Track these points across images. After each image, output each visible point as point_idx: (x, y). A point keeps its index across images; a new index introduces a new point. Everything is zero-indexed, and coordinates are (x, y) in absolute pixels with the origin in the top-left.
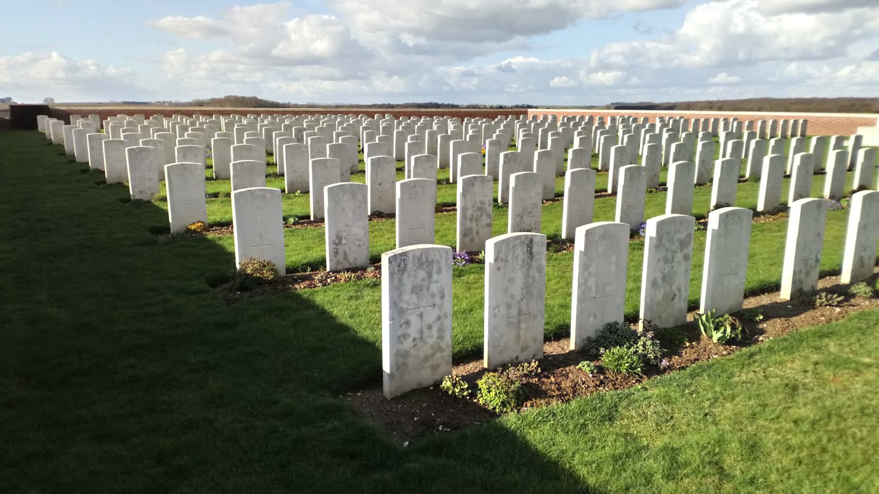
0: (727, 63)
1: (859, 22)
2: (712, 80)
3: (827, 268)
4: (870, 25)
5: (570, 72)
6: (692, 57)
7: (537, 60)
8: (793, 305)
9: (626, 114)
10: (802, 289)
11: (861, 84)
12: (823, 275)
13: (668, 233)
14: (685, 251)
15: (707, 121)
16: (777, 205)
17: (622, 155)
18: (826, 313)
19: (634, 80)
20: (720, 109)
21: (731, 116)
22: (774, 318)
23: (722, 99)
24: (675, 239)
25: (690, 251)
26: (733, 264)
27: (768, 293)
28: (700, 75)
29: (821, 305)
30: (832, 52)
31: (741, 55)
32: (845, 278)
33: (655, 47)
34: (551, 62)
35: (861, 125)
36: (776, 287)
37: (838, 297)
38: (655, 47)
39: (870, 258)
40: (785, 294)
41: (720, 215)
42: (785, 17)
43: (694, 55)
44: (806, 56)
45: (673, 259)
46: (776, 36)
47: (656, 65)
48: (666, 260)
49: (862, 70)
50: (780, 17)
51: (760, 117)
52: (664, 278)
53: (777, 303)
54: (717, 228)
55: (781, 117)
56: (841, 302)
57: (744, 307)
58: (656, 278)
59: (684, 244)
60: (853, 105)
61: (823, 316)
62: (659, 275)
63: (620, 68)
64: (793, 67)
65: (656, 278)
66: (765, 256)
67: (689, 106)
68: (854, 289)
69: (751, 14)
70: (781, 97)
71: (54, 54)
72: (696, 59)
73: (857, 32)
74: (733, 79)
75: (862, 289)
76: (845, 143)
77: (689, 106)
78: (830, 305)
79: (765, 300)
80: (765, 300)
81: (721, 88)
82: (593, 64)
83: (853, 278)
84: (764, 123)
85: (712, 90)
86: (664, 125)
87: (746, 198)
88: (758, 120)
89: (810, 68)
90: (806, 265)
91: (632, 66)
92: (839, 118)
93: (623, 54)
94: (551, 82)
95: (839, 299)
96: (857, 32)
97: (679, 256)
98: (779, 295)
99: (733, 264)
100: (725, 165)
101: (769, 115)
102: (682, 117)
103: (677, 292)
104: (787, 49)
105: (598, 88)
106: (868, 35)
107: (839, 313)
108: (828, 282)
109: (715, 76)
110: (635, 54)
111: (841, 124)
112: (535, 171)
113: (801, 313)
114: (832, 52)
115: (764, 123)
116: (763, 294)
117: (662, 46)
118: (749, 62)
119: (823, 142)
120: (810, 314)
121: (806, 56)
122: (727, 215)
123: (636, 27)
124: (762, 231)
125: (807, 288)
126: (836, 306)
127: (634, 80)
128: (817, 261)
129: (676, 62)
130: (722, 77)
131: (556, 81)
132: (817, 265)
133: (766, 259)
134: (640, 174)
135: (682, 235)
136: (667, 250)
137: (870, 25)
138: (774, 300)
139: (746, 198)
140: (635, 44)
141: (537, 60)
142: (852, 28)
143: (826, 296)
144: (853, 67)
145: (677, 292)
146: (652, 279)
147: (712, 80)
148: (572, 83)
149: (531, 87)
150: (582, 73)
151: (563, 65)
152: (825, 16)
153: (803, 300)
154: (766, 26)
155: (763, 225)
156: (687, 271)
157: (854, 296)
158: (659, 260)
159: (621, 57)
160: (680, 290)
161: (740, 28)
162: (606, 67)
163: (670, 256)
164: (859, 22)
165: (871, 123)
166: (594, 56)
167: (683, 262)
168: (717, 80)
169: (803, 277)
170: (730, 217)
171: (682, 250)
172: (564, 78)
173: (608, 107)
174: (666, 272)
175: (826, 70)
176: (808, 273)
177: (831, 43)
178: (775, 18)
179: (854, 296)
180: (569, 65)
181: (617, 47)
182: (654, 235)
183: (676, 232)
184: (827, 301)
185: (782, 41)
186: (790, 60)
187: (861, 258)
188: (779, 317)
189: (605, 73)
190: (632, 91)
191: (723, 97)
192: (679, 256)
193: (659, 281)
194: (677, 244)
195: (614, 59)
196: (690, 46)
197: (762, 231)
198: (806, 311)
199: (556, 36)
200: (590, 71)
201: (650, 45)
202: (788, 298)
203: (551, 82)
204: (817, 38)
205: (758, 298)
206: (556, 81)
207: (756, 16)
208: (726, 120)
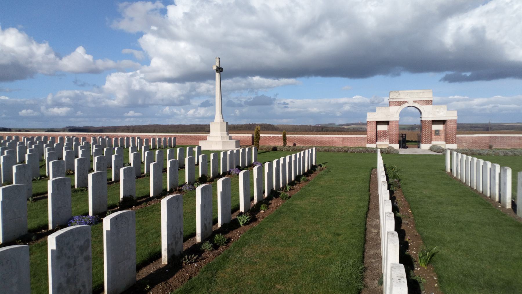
0: (133, 105)
1: (193, 89)
2: (126, 115)
4: (198, 90)
5: (34, 107)
6: (113, 101)
7: (7, 98)
10: (174, 254)
11: (198, 118)
12: (185, 240)
14: (85, 254)
15: (122, 139)
16: (161, 191)
18: (191, 267)
19: (79, 113)
20: (133, 131)
21: (137, 136)
22: (157, 284)
23: (134, 125)
25: (90, 252)
27: (155, 260)
28: (119, 112)
29: (186, 264)
30: (184, 102)
33: (90, 94)
34: (19, 100)
35: (201, 140)
37: (195, 256)
38: (90, 94)
39: (209, 223)
41: (111, 220)
42: (159, 84)
43: (114, 100)
44: (172, 104)
45: (75, 262)
47: (93, 105)
48: (68, 266)
49: (198, 111)
51: (152, 136)
52: (68, 281)
54: (109, 229)
55: (163, 136)
56: (197, 258)
57: (138, 279)
58: (60, 284)
60: (197, 128)
61: (187, 272)
63: (68, 105)
64: (167, 109)
65: (60, 284)
67: (115, 129)
69: (142, 80)
70: (162, 124)
71: (80, 50)
72: (115, 102)
73: (193, 93)
74: (136, 114)
75: (207, 246)
76: (194, 149)
77: (115, 129)
78: (191, 263)
79: (152, 268)
80: (152, 268)
81: (132, 119)
82: (50, 103)
85: (127, 120)
87: (144, 188)
88: (150, 138)
91: (76, 104)
92: (190, 136)
94: (20, 113)
96: (193, 93)
97: (80, 259)
98: (161, 262)
99: (126, 252)
100: (126, 172)
103: (81, 288)
104: (163, 100)
105: (55, 117)
106: (198, 95)
107: (196, 267)
109: (128, 112)
110: (77, 98)
111: (191, 139)
112: (26, 163)
113: (174, 275)
114: (184, 102)
117: (93, 94)
118: (144, 106)
119: (183, 151)
120: (180, 272)
122: (116, 218)
123: (75, 82)
124: (152, 212)
125: (177, 253)
126: (194, 262)
127: (79, 113)
129: (104, 104)
130: (131, 113)
134: (65, 184)
135: (81, 242)
136: (69, 258)
137: (198, 90)
138: (158, 267)
140: (78, 92)
141: (7, 98)
142: (191, 91)
143: (188, 258)
144: (194, 110)
145: (81, 288)
147: (126, 115)
148: (36, 114)
149: (4, 116)
150: (43, 108)
151: (27, 102)
152: (177, 84)
153: (176, 261)
154: (152, 87)
155: (153, 206)
156: (88, 269)
157: (203, 251)
158: (62, 267)
159: (68, 99)
160: (84, 286)
162: (60, 105)
164: (193, 89)
165: (205, 139)
166: (50, 98)
168: (129, 115)
172: (29, 111)
173: (64, 130)
174: (69, 275)
176: (176, 243)
177: (182, 98)
178: (154, 84)
179: (203, 251)
180: (32, 102)
181: (65, 93)
183: (75, 241)
184: (189, 260)
185: (159, 96)
187: (205, 224)
188: (160, 282)
190: (79, 120)
191: (134, 124)
192: (80, 259)
194: (77, 250)
195: (64, 100)
196: (111, 96)
197: (152, 212)
199: (17, 84)
200: (48, 107)
201: (86, 93)
202: (167, 263)
203: (20, 113)
204: (175, 95)
205: (148, 267)
207: (144, 82)
208: (133, 139)
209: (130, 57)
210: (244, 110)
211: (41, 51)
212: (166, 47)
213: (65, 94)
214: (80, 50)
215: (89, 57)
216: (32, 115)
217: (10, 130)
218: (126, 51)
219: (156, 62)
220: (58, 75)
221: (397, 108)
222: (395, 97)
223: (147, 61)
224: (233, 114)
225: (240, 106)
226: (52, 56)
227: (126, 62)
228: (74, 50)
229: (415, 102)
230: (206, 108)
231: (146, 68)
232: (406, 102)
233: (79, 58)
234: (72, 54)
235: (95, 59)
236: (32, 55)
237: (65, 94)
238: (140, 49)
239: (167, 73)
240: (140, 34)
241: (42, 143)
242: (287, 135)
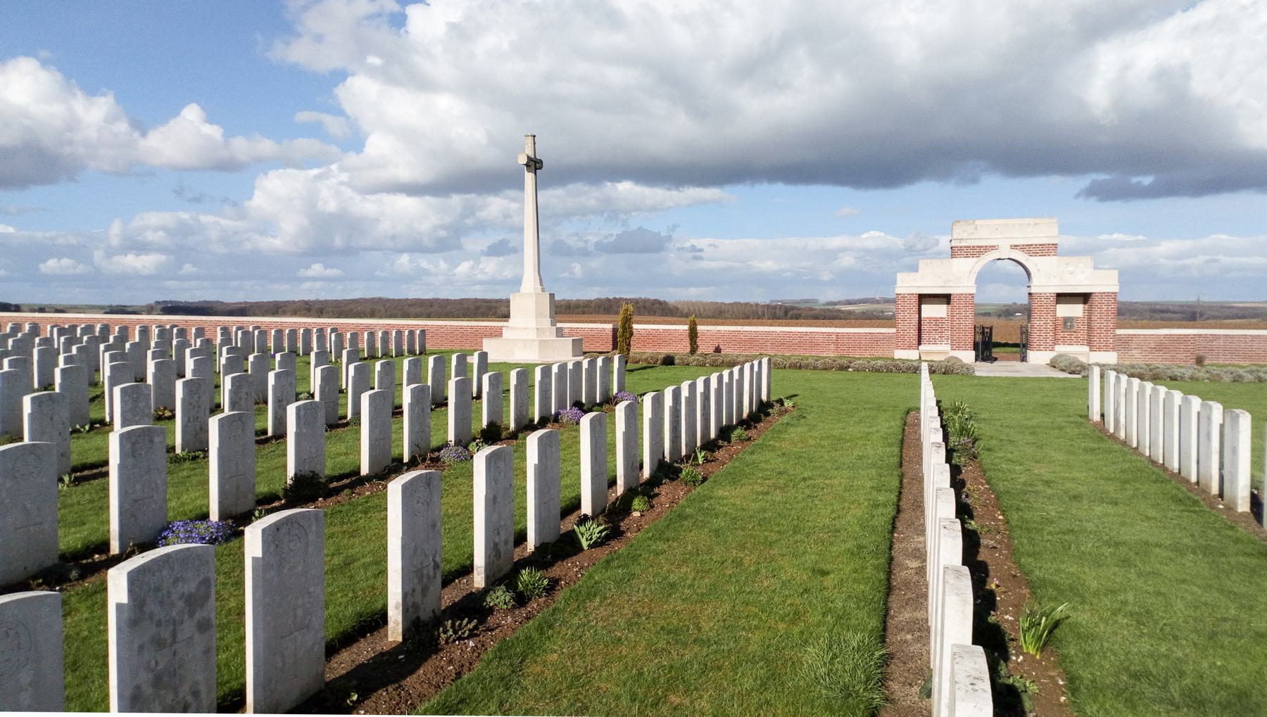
0: (320, 251)
1: (470, 211)
3: (453, 566)
4: (482, 215)
5: (78, 252)
6: (272, 240)
7: (11, 230)
8: (407, 653)
9: (169, 321)
10: (418, 618)
12: (447, 581)
13: (157, 589)
14: (199, 615)
15: (293, 333)
16: (389, 462)
17: (136, 401)
18: (458, 649)
19: (188, 268)
21: (329, 325)
22: (376, 691)
23: (322, 299)
24: (174, 597)
26: (299, 612)
27: (371, 632)
29: (447, 642)
30: (446, 243)
31: (338, 242)
32: (479, 580)
33: (215, 223)
35: (486, 336)
36: (380, 619)
37: (469, 622)
38: (215, 223)
39: (506, 542)
40: (395, 630)
41: (264, 531)
43: (274, 237)
44: (416, 247)
46: (377, 220)
47: (222, 250)
48: (158, 643)
50: (379, 196)
51: (368, 326)
52: (157, 682)
53: (382, 654)
55: (393, 326)
56: (476, 628)
57: (329, 676)
59: (194, 602)
61: (450, 662)
62: (144, 677)
63: (161, 249)
64: (405, 259)
66: (368, 560)
67: (276, 309)
68: (490, 601)
69: (343, 188)
72: (277, 243)
73: (470, 222)
77: (276, 309)
78: (460, 638)
79: (363, 651)
80: (363, 651)
81: (319, 284)
82: (115, 241)
83: (487, 578)
84: (372, 335)
85: (306, 285)
86: (227, 339)
87: (346, 454)
89: (424, 262)
90: (421, 578)
91: (182, 247)
93: (165, 229)
94: (41, 266)
95: (471, 626)
96: (470, 222)
97: (188, 628)
98: (386, 636)
99: (299, 612)
100: (302, 413)
101: (379, 323)
102: (256, 328)
104: (393, 238)
106: (481, 227)
107: (473, 650)
108: (451, 596)
109: (308, 267)
110: (183, 230)
113: (418, 667)
114: (446, 243)
115: (372, 335)
116: (364, 636)
118: (349, 251)
119: (441, 363)
121: (416, 247)
122: (277, 527)
123: (179, 192)
124: (366, 513)
125: (425, 615)
126: (468, 638)
127: (188, 268)
128: (436, 566)
129: (248, 246)
130: (317, 269)
131: (51, 265)
132: (436, 567)
133: (370, 564)
134: (151, 441)
135: (190, 587)
136: (159, 623)
137: (482, 215)
139: (346, 454)
140: (185, 216)
141: (11, 230)
143: (453, 626)
144: (471, 262)
146: (128, 693)
148: (81, 269)
150: (98, 255)
152: (429, 199)
153: (423, 636)
154: (367, 207)
155: (368, 499)
157: (491, 611)
158: (141, 647)
159: (161, 233)
161: (331, 206)
162: (140, 247)
163: (166, 634)
164: (470, 211)
165: (497, 334)
166: (116, 229)
167: (197, 637)
168: (310, 273)
169: (418, 599)
170: (283, 531)
171: (192, 614)
172: (66, 262)
173: (150, 310)
174: (161, 667)
175: (443, 265)
176: (425, 590)
177: (442, 233)
178: (374, 197)
179: (491, 611)
180: (72, 240)
182: (124, 599)
183: (176, 581)
184: (455, 632)
185: (385, 227)
186: (401, 251)
187: (496, 545)
188: (384, 685)
189: (138, 255)
190: (187, 284)
191: (324, 296)
192: (188, 628)
193: (148, 690)
194: (181, 604)
195: (150, 236)
196: (267, 226)
198: (426, 660)
199: (34, 195)
200: (111, 252)
201: (204, 219)
202: (400, 639)
203: (41, 266)
204: (425, 226)
205: (354, 648)
206: (51, 265)
207: (349, 192)
209: (315, 130)
210: (595, 263)
211: (94, 115)
212: (402, 106)
213: (155, 222)
214: (192, 113)
215: (214, 132)
216: (71, 271)
217: (17, 308)
218: (304, 116)
219: (378, 145)
220: (137, 175)
221: (971, 261)
222: (965, 236)
223: (355, 142)
224: (566, 275)
225: (585, 253)
226: (122, 127)
227: (304, 145)
228: (176, 113)
229: (1015, 247)
230: (501, 259)
231: (352, 159)
232: (993, 248)
233: (187, 132)
234: (172, 123)
235: (229, 134)
236: (73, 124)
237: (155, 222)
238: (338, 111)
239: (405, 172)
240: (340, 76)
241: (95, 341)
242: (699, 328)
